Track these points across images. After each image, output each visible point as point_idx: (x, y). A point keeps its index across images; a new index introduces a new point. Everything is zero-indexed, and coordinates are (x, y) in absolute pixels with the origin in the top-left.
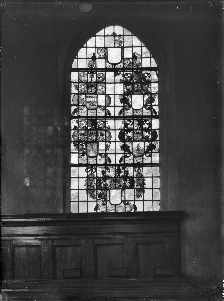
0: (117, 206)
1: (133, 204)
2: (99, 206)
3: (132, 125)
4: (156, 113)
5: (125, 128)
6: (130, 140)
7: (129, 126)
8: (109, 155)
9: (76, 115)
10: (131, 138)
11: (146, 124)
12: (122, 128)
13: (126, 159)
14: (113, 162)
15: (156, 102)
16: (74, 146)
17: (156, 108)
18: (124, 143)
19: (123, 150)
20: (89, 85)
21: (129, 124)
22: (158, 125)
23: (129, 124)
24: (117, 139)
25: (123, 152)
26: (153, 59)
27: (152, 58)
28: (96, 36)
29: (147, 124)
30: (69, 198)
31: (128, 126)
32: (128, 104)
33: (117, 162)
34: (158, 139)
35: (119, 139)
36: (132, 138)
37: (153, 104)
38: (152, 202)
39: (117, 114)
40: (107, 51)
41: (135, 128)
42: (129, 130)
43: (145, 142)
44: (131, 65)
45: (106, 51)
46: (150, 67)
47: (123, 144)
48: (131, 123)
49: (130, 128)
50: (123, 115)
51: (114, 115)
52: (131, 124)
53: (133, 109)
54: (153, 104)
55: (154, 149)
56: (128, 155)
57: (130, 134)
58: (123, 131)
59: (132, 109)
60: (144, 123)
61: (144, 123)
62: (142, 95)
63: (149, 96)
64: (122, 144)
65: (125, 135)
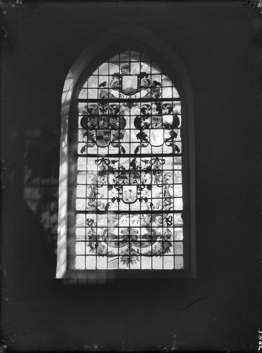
1: (150, 203)
3: (150, 110)
4: (178, 151)
5: (142, 114)
6: (147, 126)
8: (122, 145)
9: (84, 153)
11: (166, 108)
12: (139, 114)
13: (143, 149)
15: (179, 138)
16: (84, 135)
17: (179, 145)
19: (139, 139)
20: (100, 119)
21: (146, 109)
22: (182, 221)
23: (146, 109)
24: (133, 126)
25: (139, 141)
26: (174, 89)
27: (174, 86)
28: (109, 62)
29: (167, 108)
31: (145, 111)
32: (146, 140)
34: (180, 126)
35: (135, 126)
36: (151, 125)
38: (173, 257)
39: (133, 152)
41: (154, 113)
44: (149, 95)
45: (121, 79)
46: (172, 98)
48: (149, 108)
51: (129, 153)
52: (149, 109)
53: (152, 146)
55: (175, 138)
56: (145, 144)
57: (148, 121)
60: (164, 107)
61: (164, 107)
63: (170, 131)
64: (138, 131)
65: (142, 122)
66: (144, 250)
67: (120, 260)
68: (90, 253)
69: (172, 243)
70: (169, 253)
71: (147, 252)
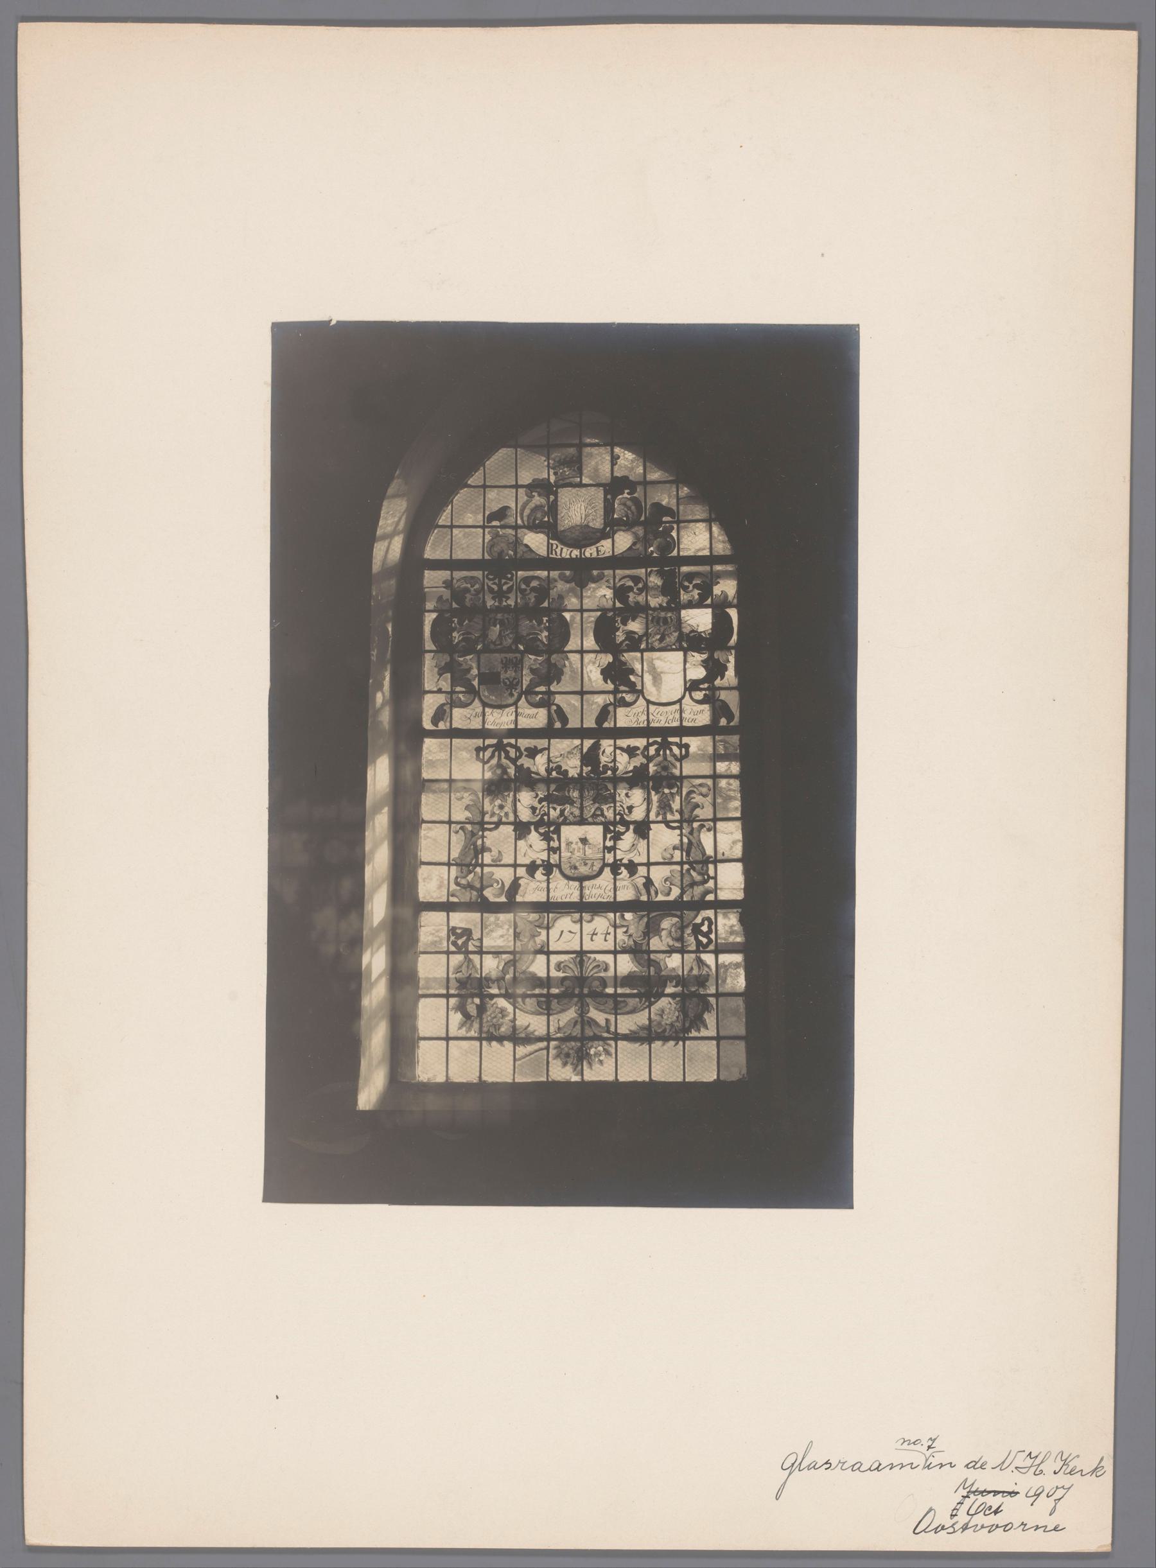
0: (586, 884)
2: (520, 882)
4: (730, 716)
7: (632, 597)
8: (558, 699)
9: (442, 726)
10: (641, 637)
14: (574, 723)
17: (732, 699)
18: (615, 658)
21: (630, 589)
24: (590, 642)
25: (610, 686)
27: (715, 520)
29: (696, 586)
30: (415, 940)
33: (590, 723)
37: (718, 682)
39: (590, 723)
40: (556, 500)
42: (632, 612)
43: (690, 653)
45: (552, 498)
47: (610, 658)
48: (640, 585)
49: (637, 603)
50: (612, 725)
53: (649, 702)
54: (718, 682)
56: (629, 698)
57: (635, 626)
58: (610, 614)
59: (645, 703)
61: (686, 584)
62: (681, 654)
66: (626, 1024)
67: (552, 1052)
68: (462, 1032)
69: (712, 1000)
70: (704, 1033)
71: (634, 1028)
